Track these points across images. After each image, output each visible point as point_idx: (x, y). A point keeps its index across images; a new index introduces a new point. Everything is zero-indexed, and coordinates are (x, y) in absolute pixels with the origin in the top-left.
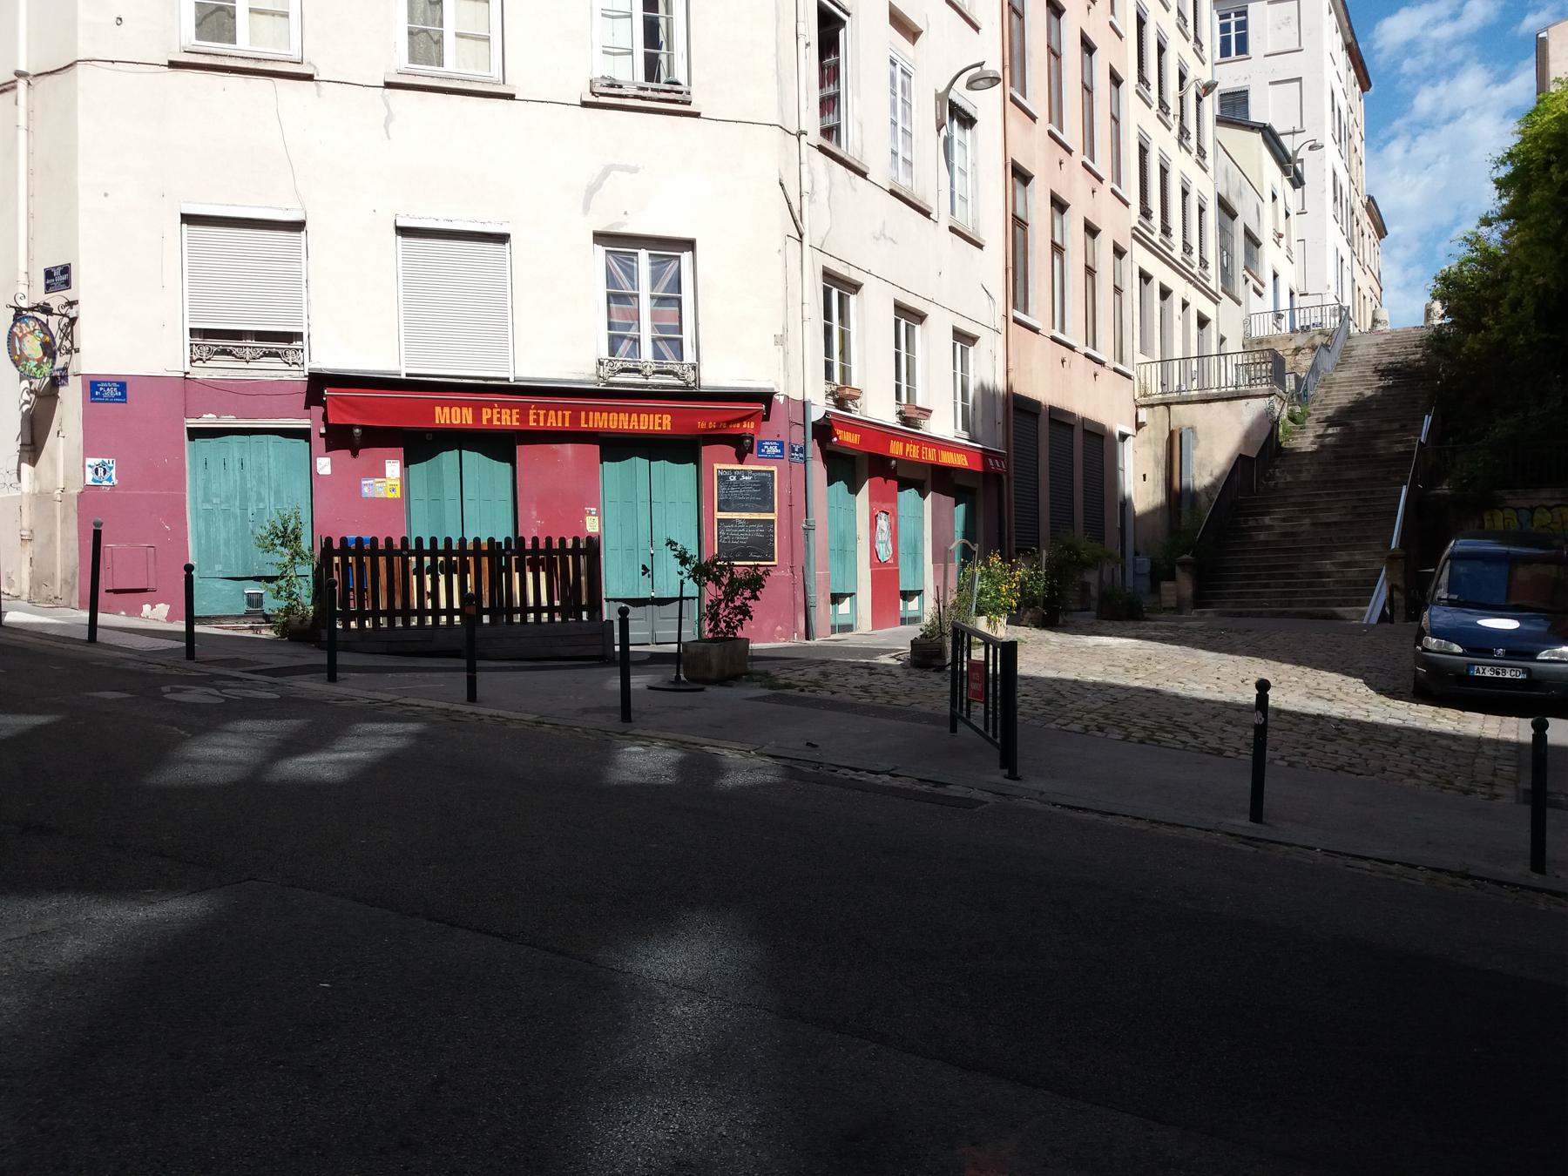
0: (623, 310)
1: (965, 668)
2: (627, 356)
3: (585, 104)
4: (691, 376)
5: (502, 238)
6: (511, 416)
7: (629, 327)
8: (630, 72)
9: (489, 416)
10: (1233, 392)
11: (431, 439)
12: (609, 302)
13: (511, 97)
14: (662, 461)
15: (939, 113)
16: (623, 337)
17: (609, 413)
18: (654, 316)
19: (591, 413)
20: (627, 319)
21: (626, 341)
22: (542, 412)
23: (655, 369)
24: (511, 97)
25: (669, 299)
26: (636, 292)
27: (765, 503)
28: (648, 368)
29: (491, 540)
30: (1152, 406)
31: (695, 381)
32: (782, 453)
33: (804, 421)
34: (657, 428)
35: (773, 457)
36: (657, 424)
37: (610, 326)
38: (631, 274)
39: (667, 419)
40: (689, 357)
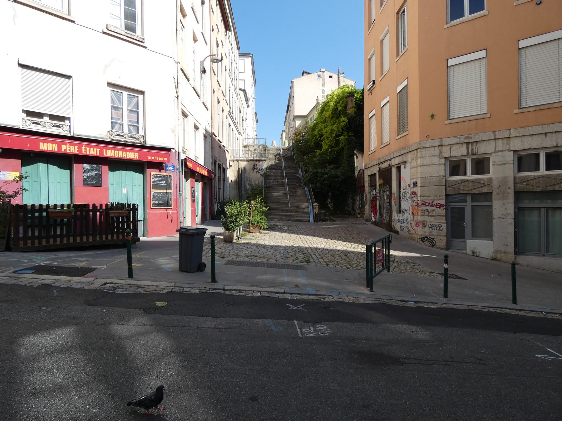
0: (117, 113)
1: (384, 250)
2: (118, 130)
3: (104, 33)
4: (142, 140)
5: (69, 77)
6: (75, 149)
7: (119, 119)
8: (118, 24)
9: (65, 148)
10: (252, 159)
11: (31, 154)
12: (111, 109)
13: (74, 22)
14: (131, 172)
15: (201, 67)
16: (116, 123)
17: (115, 151)
18: (129, 117)
19: (108, 150)
20: (118, 117)
21: (117, 125)
22: (88, 149)
23: (129, 136)
24: (74, 22)
25: (135, 111)
26: (122, 107)
27: (167, 187)
28: (127, 135)
29: (123, 203)
30: (234, 161)
31: (144, 142)
32: (174, 170)
33: (179, 159)
34: (133, 158)
35: (171, 171)
36: (133, 156)
37: (112, 118)
38: (120, 101)
39: (137, 155)
40: (141, 132)
